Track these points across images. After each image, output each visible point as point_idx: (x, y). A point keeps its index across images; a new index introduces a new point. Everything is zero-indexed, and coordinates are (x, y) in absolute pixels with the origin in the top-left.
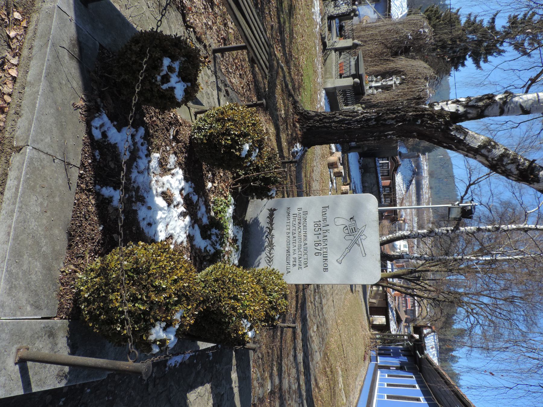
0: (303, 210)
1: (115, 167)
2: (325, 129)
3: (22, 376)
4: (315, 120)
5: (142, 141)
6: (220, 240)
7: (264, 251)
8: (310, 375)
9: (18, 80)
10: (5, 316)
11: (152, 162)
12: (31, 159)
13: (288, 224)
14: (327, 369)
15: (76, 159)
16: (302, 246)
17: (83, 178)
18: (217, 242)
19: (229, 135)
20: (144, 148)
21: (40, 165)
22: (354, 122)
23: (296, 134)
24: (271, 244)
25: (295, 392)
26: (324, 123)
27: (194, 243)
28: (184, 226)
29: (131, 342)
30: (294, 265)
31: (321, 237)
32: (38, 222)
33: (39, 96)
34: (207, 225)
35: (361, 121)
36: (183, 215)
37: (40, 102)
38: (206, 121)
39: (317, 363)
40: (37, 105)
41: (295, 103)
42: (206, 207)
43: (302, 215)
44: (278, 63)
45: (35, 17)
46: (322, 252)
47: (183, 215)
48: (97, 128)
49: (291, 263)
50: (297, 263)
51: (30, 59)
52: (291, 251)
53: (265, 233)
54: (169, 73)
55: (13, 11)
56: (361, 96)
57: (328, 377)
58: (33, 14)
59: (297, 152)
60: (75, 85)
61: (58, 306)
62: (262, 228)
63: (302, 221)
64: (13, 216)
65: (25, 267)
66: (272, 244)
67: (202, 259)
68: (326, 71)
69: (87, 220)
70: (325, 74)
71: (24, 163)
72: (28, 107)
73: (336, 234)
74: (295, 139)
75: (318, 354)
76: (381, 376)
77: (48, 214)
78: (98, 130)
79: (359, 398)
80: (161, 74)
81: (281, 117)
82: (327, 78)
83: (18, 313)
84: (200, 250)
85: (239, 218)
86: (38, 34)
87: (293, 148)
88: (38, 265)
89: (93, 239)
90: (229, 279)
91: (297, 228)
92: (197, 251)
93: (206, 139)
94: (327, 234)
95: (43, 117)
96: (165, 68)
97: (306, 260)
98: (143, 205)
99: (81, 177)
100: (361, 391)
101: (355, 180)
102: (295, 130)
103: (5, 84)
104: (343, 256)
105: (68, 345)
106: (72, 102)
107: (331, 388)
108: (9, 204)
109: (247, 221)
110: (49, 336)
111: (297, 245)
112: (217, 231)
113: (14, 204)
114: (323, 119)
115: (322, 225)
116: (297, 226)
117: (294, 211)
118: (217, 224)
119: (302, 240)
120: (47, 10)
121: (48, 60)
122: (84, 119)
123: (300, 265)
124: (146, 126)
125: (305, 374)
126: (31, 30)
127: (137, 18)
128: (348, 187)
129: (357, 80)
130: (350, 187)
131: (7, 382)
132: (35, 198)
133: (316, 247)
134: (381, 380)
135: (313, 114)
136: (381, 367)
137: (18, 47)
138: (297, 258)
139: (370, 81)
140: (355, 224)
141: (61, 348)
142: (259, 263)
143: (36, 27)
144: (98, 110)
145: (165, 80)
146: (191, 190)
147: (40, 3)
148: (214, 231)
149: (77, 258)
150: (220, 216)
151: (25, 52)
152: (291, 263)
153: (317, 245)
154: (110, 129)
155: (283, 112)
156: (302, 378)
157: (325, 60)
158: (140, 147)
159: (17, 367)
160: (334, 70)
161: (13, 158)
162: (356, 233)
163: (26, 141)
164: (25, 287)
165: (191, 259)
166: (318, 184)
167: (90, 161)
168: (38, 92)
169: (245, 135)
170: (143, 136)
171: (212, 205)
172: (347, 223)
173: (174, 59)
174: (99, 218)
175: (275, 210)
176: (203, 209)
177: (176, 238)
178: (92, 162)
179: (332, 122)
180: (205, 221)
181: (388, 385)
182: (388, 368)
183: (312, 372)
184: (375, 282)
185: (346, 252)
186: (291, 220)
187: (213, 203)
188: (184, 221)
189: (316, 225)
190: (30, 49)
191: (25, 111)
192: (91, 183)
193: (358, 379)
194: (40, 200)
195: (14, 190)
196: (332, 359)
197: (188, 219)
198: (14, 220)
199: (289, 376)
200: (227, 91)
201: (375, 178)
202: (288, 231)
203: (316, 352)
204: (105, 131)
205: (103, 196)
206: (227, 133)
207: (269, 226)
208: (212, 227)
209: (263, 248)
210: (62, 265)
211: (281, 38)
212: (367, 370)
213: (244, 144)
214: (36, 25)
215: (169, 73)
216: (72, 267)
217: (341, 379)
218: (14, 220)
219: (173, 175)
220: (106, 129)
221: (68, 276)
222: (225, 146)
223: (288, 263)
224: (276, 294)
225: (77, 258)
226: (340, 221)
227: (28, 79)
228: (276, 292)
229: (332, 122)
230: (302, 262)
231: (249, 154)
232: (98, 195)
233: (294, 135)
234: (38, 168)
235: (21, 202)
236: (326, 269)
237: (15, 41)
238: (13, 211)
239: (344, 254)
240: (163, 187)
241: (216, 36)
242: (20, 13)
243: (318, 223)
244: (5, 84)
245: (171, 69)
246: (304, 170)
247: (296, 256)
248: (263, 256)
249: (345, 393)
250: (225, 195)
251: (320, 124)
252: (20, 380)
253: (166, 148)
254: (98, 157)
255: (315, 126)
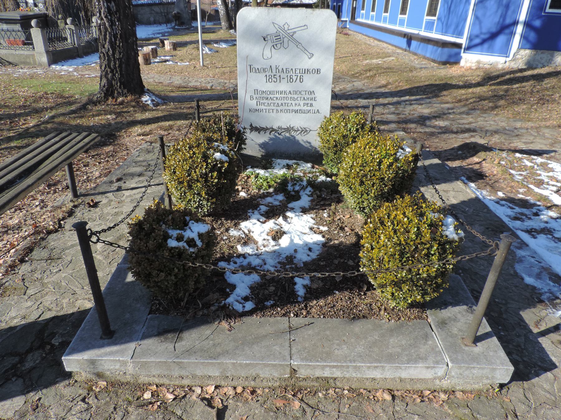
0: (253, 95)
1: (273, 286)
2: (123, 66)
3: (484, 340)
4: (113, 79)
5: (232, 263)
6: (297, 181)
7: (295, 137)
8: (377, 93)
9: (218, 384)
10: (444, 359)
11: (248, 252)
12: (302, 360)
13: (267, 111)
14: (368, 74)
15: (282, 323)
16: (292, 96)
17: (297, 313)
18: (300, 185)
19: (206, 174)
20: (238, 260)
21: (304, 351)
22: (113, 30)
23: (131, 101)
24: (288, 130)
25: (396, 108)
26: (115, 68)
27: (307, 206)
28: (297, 217)
29: (480, 254)
30: (311, 105)
31: (283, 75)
32: (356, 346)
33: (239, 362)
34: (284, 195)
35: (111, 20)
36: (285, 218)
37: (244, 360)
38: (190, 200)
39: (364, 85)
40: (248, 362)
41: (91, 102)
42: (267, 196)
43: (258, 96)
44: (47, 122)
45: (143, 379)
46: (299, 75)
47: (285, 218)
48: (244, 307)
49: (309, 108)
50: (310, 102)
51: (194, 377)
52: (297, 108)
53: (275, 136)
54: (185, 239)
55: (144, 399)
56: (48, 18)
57: (375, 75)
58: (139, 381)
59: (152, 101)
60: (208, 332)
61: (418, 320)
62: (271, 139)
63: (264, 95)
64: (360, 366)
65: (399, 350)
66: (288, 128)
67: (321, 199)
68: (25, 63)
69: (334, 306)
70: (29, 64)
71: (309, 365)
72: (249, 370)
73: (280, 58)
74: (138, 102)
75: (355, 84)
76: (362, 18)
77: (345, 338)
78: (245, 305)
79: (386, 43)
80: (187, 247)
81: (115, 119)
82: (34, 61)
83: (437, 349)
84: (312, 201)
85: (266, 162)
86: (166, 373)
87: (148, 105)
88: (393, 341)
89: (350, 298)
90: (361, 170)
91: (273, 101)
92: (314, 203)
93: (212, 199)
94: (280, 69)
95: (257, 356)
96: (181, 244)
97: (307, 93)
98: (295, 257)
99: (297, 315)
100: (379, 41)
101: (150, 33)
102: (128, 102)
103: (225, 394)
104: (306, 52)
105: (446, 308)
106: (228, 332)
107: (386, 72)
108: (348, 372)
109: (262, 155)
110: (446, 324)
111: (290, 102)
112: (289, 185)
113: (348, 367)
114: (110, 67)
115: (270, 73)
116: (270, 102)
117: (253, 104)
118: (282, 186)
119: (285, 96)
120: (137, 369)
121: (196, 359)
122: (239, 319)
123: (311, 99)
124: (215, 260)
125: (378, 98)
126: (160, 380)
127: (81, 282)
128: (166, 42)
129: (33, 22)
130: (166, 40)
131: (492, 350)
132: (336, 351)
133: (294, 81)
134: (367, 18)
135: (104, 81)
136: (353, 17)
137: (181, 389)
138: (304, 102)
139: (27, 6)
140: (271, 35)
141: (451, 314)
142: (307, 142)
143: (156, 376)
144: (225, 308)
145: (191, 243)
146: (256, 212)
147: (127, 377)
148: (290, 188)
149: (372, 310)
150: (273, 183)
151: (186, 382)
152: (309, 108)
153: (291, 80)
154: (238, 294)
155: (109, 116)
156: (381, 101)
157: (10, 63)
158: (238, 264)
159: (478, 344)
160: (22, 52)
161: (301, 375)
162: (281, 34)
163: (285, 367)
164: (415, 347)
165: (325, 209)
166: (173, 77)
167: (279, 309)
168: (234, 364)
169: (205, 157)
170: (227, 263)
171: (262, 191)
172: (270, 44)
173: (167, 237)
174: (329, 294)
175: (251, 125)
176: (269, 199)
177: (311, 225)
178: (278, 307)
179: (114, 57)
180: (281, 197)
181: (373, 10)
182: (354, 10)
183: (374, 91)
184: (336, 17)
185: (301, 47)
186: (263, 107)
187: (259, 189)
188: (292, 218)
189: (270, 80)
190: (183, 378)
191: (253, 372)
192: (299, 306)
193: (369, 43)
194: (335, 346)
195: (334, 369)
196: (357, 69)
197: (289, 214)
198: (363, 365)
199: (383, 114)
200: (119, 180)
201: (144, 8)
202: (275, 111)
203: (353, 85)
204: (242, 299)
205: (305, 294)
206: (205, 176)
207: (268, 132)
208: (286, 190)
209: (292, 138)
210: (383, 321)
211: (6, 118)
212: (357, 32)
213: (215, 159)
214: (154, 376)
215: (185, 239)
216: (382, 312)
217: (374, 61)
218: (363, 365)
219: (249, 231)
220: (240, 298)
221: (391, 315)
222: (219, 178)
223: (309, 111)
224: (348, 125)
225: (372, 310)
226: (267, 53)
227: (217, 374)
228: (346, 124)
229: (114, 57)
230: (308, 96)
231: (223, 152)
232: (307, 299)
233: (134, 103)
234: (308, 352)
235: (345, 362)
236: (318, 71)
237: (176, 393)
238: (355, 367)
239: (303, 50)
240: (268, 240)
241: (50, 195)
242: (144, 393)
243: (268, 78)
244: (225, 394)
245: (180, 238)
246: (168, 94)
247: (302, 103)
248: (300, 138)
249: (386, 57)
250: (246, 178)
251: (117, 72)
252: (487, 340)
253: (226, 239)
254: (272, 302)
255: (120, 79)
